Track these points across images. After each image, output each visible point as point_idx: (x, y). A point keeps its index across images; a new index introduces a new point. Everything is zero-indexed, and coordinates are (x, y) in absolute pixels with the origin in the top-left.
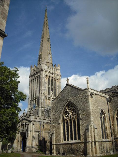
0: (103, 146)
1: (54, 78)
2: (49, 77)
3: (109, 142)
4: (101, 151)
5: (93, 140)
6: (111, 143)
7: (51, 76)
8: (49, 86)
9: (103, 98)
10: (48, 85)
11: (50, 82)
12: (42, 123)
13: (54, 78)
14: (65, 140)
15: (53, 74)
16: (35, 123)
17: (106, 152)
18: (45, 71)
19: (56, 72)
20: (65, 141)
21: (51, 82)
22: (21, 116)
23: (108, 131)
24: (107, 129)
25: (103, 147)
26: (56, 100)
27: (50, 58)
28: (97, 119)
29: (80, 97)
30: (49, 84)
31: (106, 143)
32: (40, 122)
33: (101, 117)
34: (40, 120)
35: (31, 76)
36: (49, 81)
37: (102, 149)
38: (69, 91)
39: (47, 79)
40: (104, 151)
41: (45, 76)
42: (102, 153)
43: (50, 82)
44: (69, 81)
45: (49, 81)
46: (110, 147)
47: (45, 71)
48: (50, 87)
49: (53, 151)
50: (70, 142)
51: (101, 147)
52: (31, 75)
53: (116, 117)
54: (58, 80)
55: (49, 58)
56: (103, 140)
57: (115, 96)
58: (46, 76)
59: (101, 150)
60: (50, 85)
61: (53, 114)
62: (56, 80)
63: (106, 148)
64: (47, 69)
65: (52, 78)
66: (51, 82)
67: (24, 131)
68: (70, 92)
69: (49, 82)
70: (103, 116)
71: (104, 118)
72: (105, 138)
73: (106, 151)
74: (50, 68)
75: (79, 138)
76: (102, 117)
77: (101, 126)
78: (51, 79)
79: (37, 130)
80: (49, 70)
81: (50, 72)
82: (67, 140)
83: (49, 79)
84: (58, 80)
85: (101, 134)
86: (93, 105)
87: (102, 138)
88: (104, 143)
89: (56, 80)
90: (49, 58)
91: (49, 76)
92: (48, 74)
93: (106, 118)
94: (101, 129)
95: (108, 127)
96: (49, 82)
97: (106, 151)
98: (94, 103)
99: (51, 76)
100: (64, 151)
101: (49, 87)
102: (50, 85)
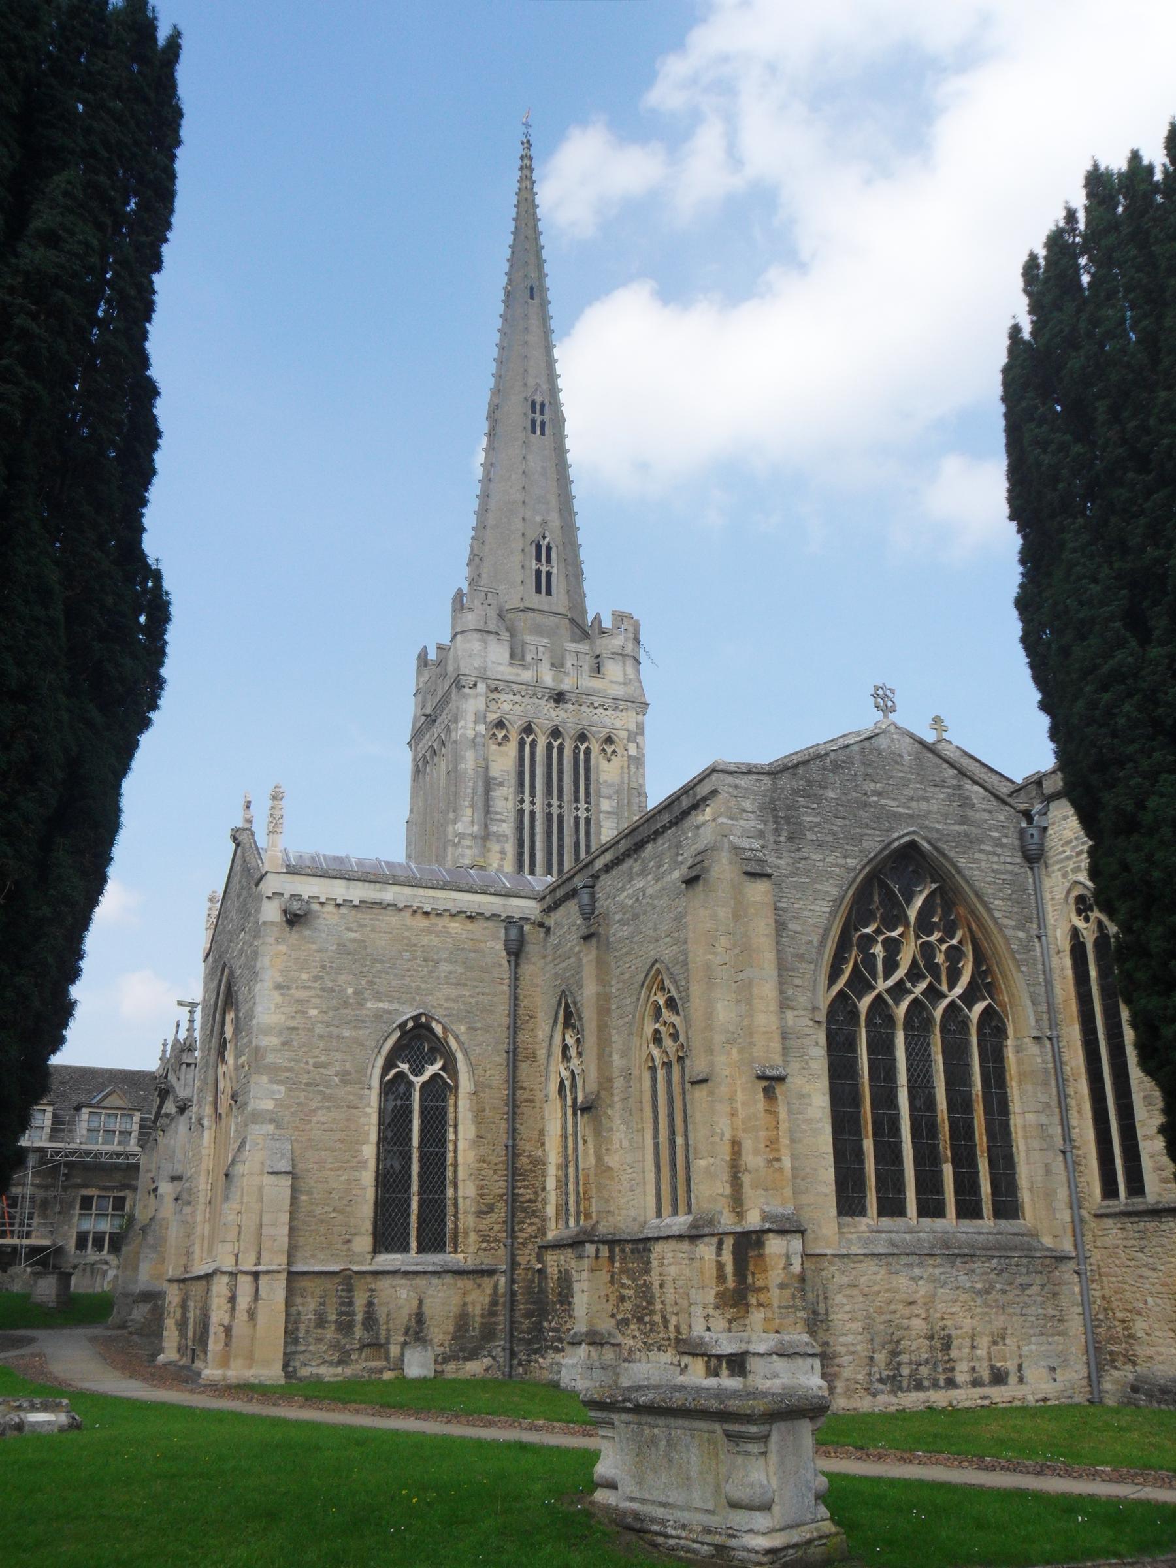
0: (370, 1304)
1: (569, 732)
2: (528, 729)
4: (336, 1346)
6: (488, 1283)
7: (550, 715)
8: (522, 801)
9: (455, 926)
13: (569, 732)
14: (659, 1214)
15: (559, 698)
18: (482, 687)
19: (589, 683)
25: (359, 1317)
27: (549, 574)
28: (329, 1098)
30: (521, 784)
31: (420, 1282)
39: (512, 748)
41: (482, 728)
42: (340, 1362)
47: (482, 687)
48: (538, 808)
51: (340, 1314)
54: (609, 740)
55: (538, 572)
58: (500, 724)
60: (533, 794)
65: (556, 733)
71: (439, 1093)
72: (413, 1244)
78: (549, 747)
80: (527, 676)
81: (534, 689)
83: (522, 743)
84: (609, 740)
87: (364, 1243)
88: (384, 1284)
89: (595, 747)
90: (538, 572)
96: (521, 774)
101: (521, 812)
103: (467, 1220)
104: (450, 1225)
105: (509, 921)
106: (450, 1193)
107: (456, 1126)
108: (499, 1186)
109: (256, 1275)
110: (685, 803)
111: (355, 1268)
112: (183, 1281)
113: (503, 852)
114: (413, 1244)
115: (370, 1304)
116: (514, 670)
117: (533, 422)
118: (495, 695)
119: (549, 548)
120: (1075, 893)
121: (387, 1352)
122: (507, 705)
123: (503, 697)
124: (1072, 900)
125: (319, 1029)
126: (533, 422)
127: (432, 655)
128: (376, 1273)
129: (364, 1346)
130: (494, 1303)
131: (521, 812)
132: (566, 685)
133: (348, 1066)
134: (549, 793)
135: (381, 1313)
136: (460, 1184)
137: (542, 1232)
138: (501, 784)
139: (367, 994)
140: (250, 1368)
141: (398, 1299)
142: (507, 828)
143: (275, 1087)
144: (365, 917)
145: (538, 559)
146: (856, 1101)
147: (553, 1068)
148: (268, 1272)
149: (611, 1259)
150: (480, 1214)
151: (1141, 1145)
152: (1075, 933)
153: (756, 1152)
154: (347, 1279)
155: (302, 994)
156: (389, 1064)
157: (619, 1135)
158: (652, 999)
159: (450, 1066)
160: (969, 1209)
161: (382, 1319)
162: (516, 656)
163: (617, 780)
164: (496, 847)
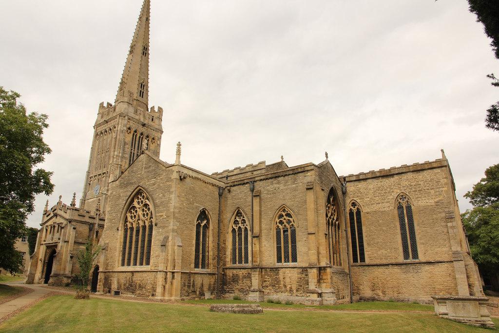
0: (194, 281)
2: (135, 131)
3: (209, 274)
5: (170, 269)
8: (132, 150)
9: (210, 187)
10: (130, 148)
11: (135, 143)
12: (96, 226)
15: (144, 125)
16: (78, 226)
17: (200, 293)
18: (126, 117)
19: (151, 123)
20: (281, 262)
21: (137, 143)
22: (52, 209)
23: (211, 253)
24: (210, 249)
26: (118, 181)
27: (143, 92)
29: (162, 179)
32: (93, 224)
33: (198, 226)
34: (91, 221)
35: (96, 126)
36: (133, 140)
37: (189, 287)
38: (144, 166)
40: (194, 292)
41: (125, 128)
42: (188, 296)
43: (135, 143)
44: (181, 147)
45: (133, 140)
46: (210, 284)
47: (126, 117)
48: (136, 152)
49: (98, 285)
50: (131, 268)
52: (98, 123)
53: (233, 227)
54: (153, 139)
55: (141, 91)
56: (196, 269)
57: (237, 185)
58: (129, 129)
59: (186, 288)
60: (134, 149)
61: (110, 209)
62: (144, 137)
63: (199, 285)
64: (132, 115)
66: (137, 143)
67: (54, 241)
68: (145, 168)
69: (132, 142)
70: (205, 222)
71: (206, 227)
72: (200, 266)
73: (198, 293)
74: (138, 113)
75: (247, 262)
76: (202, 225)
77: (194, 242)
78: (140, 137)
79: (80, 240)
80: (137, 117)
81: (138, 121)
82: (413, 258)
83: (134, 134)
84: (153, 139)
85: (193, 257)
86: (183, 199)
87: (193, 265)
90: (141, 91)
91: (134, 130)
92: (134, 126)
93: (211, 227)
94: (194, 248)
95: (211, 245)
96: (132, 142)
97: (198, 293)
98: (185, 195)
99: (141, 129)
100: (119, 287)
101: (131, 152)
102: (134, 149)
103: (211, 261)
104: (207, 262)
105: (219, 188)
106: (207, 254)
107: (208, 237)
108: (216, 253)
109: (173, 273)
110: (300, 170)
111: (192, 272)
112: (105, 272)
113: (126, 162)
114: (144, 263)
115: (194, 281)
116: (134, 115)
117: (144, 52)
118: (129, 120)
119: (144, 86)
120: (352, 202)
121: (196, 293)
122: (131, 124)
123: (131, 122)
124: (351, 203)
125: (186, 209)
126: (144, 52)
127: (105, 105)
128: (195, 273)
129: (192, 292)
130: (215, 282)
131: (131, 152)
132: (146, 122)
133: (191, 220)
134: (138, 149)
135: (196, 283)
136: (210, 252)
137: (225, 265)
138: (127, 144)
139: (194, 201)
140: (171, 297)
141: (198, 280)
142: (127, 156)
143: (177, 223)
144: (195, 181)
145: (141, 88)
146: (238, 235)
147: (230, 226)
148: (177, 272)
149: (262, 272)
150: (213, 259)
151: (365, 253)
152: (351, 209)
153: (323, 250)
154: (190, 274)
155: (183, 199)
156: (197, 220)
157: (265, 243)
158: (280, 213)
159: (208, 222)
160: (240, 262)
161: (196, 285)
162: (136, 112)
163: (154, 149)
164: (124, 161)
